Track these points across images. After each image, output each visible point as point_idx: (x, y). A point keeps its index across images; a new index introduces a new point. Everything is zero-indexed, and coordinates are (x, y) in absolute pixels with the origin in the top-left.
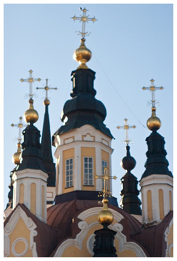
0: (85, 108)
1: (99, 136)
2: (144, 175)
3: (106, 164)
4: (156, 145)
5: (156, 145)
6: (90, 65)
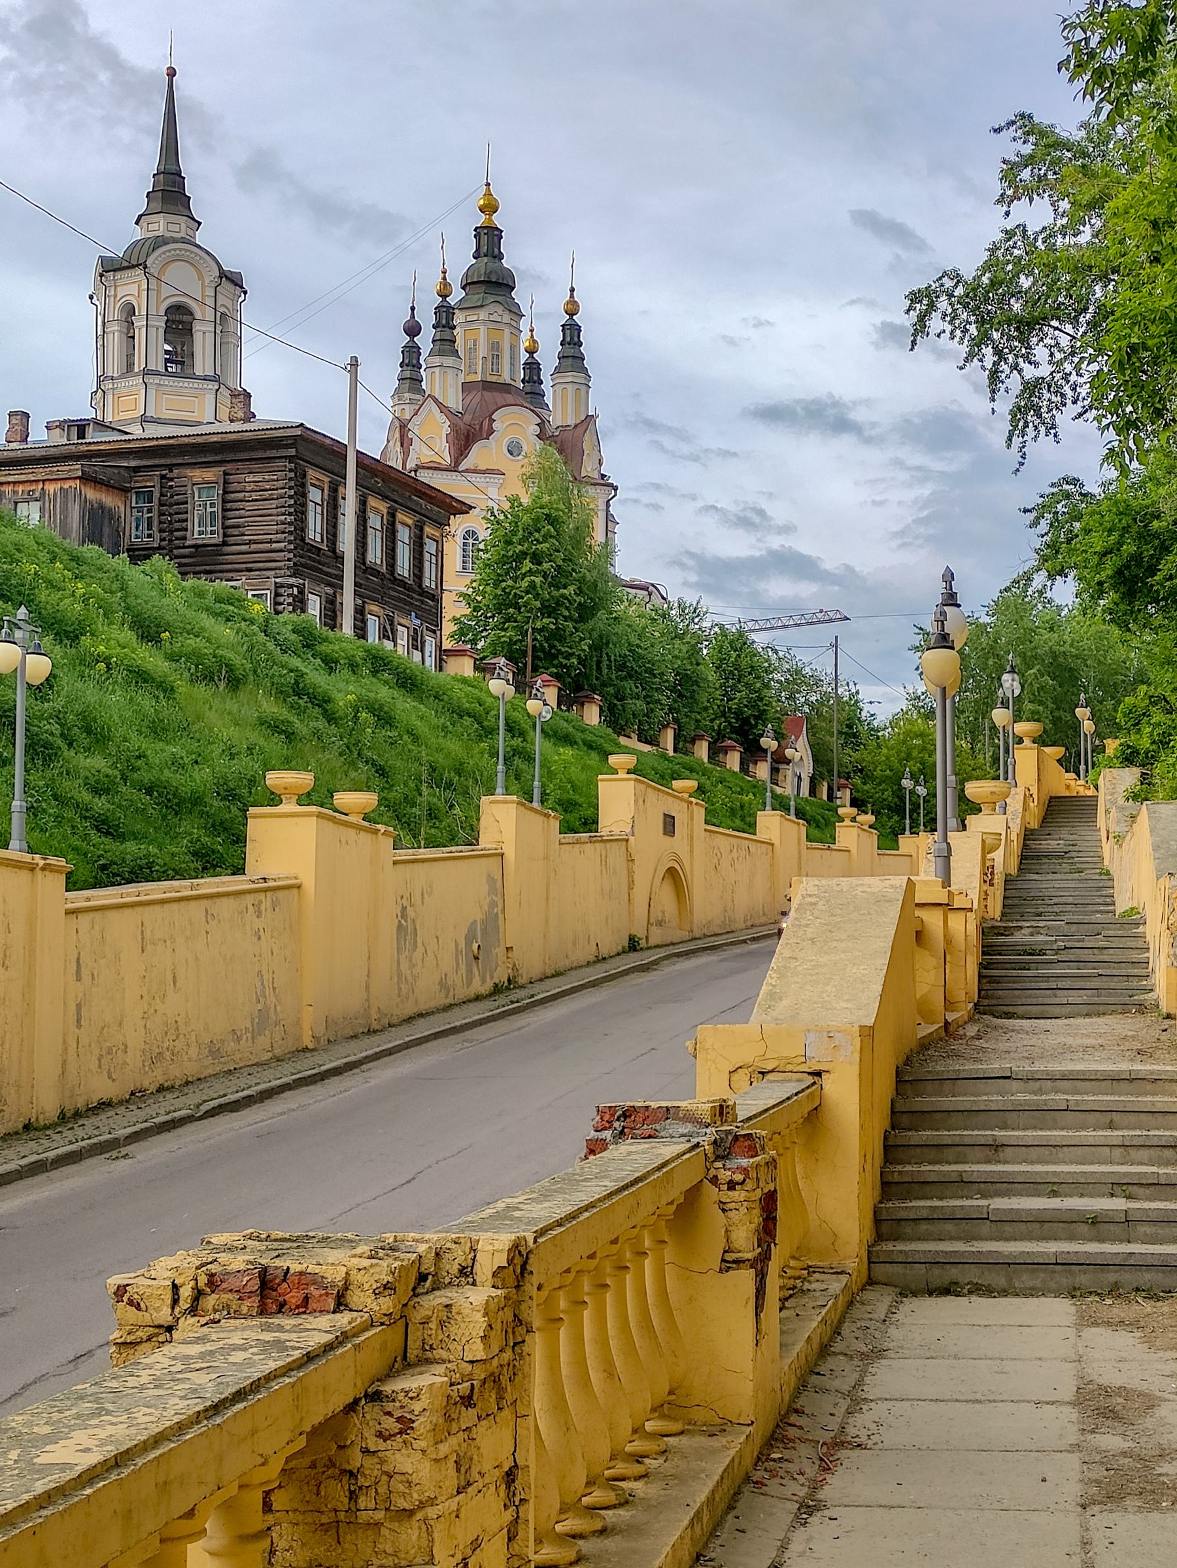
0: (492, 282)
1: (506, 318)
2: (558, 370)
3: (513, 348)
4: (572, 334)
5: (572, 334)
6: (498, 220)
